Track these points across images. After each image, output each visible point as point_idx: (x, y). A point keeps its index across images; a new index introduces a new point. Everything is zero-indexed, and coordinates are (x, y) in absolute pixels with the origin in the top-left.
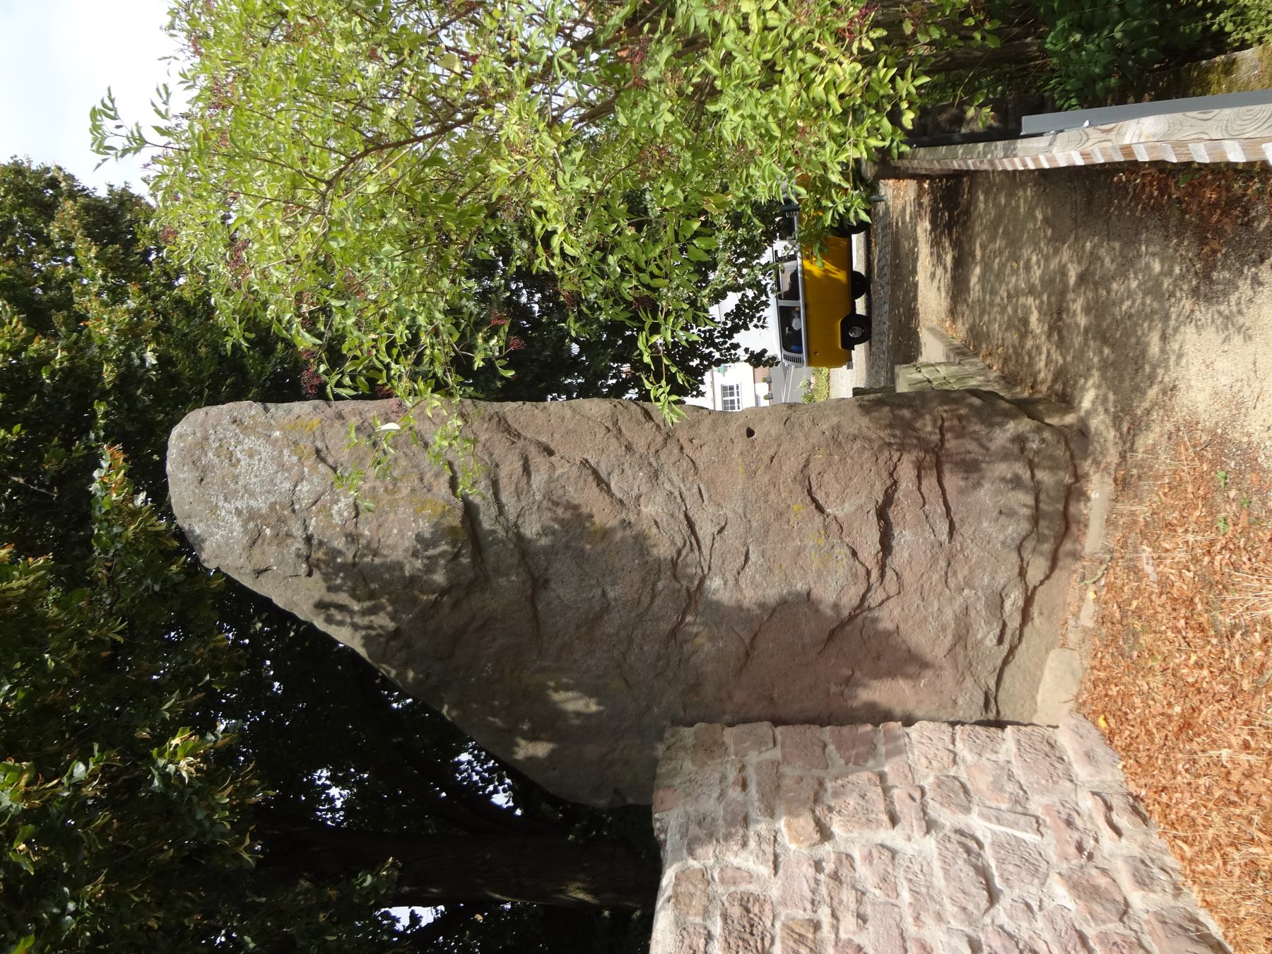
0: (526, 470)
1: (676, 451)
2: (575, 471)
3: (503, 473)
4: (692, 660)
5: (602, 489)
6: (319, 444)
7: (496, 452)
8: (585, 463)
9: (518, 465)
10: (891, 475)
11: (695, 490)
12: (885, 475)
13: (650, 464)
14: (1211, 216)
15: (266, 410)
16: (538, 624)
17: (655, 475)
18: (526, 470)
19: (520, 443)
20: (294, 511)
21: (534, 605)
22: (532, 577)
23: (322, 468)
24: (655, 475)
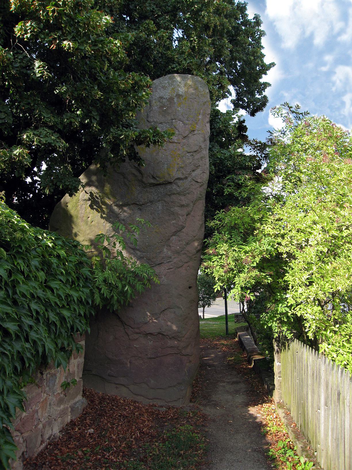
0: (182, 206)
1: (185, 261)
2: (180, 223)
3: (182, 198)
4: (174, 197)
5: (174, 233)
6: (195, 132)
7: (189, 196)
8: (183, 227)
9: (184, 203)
10: (173, 337)
11: (171, 267)
12: (173, 335)
13: (181, 251)
14: (186, 1)
15: (207, 123)
16: (166, 184)
17: (178, 253)
18: (182, 206)
19: (191, 204)
20: (173, 119)
21: (133, 204)
22: (143, 204)
23: (187, 133)
24: (178, 253)
